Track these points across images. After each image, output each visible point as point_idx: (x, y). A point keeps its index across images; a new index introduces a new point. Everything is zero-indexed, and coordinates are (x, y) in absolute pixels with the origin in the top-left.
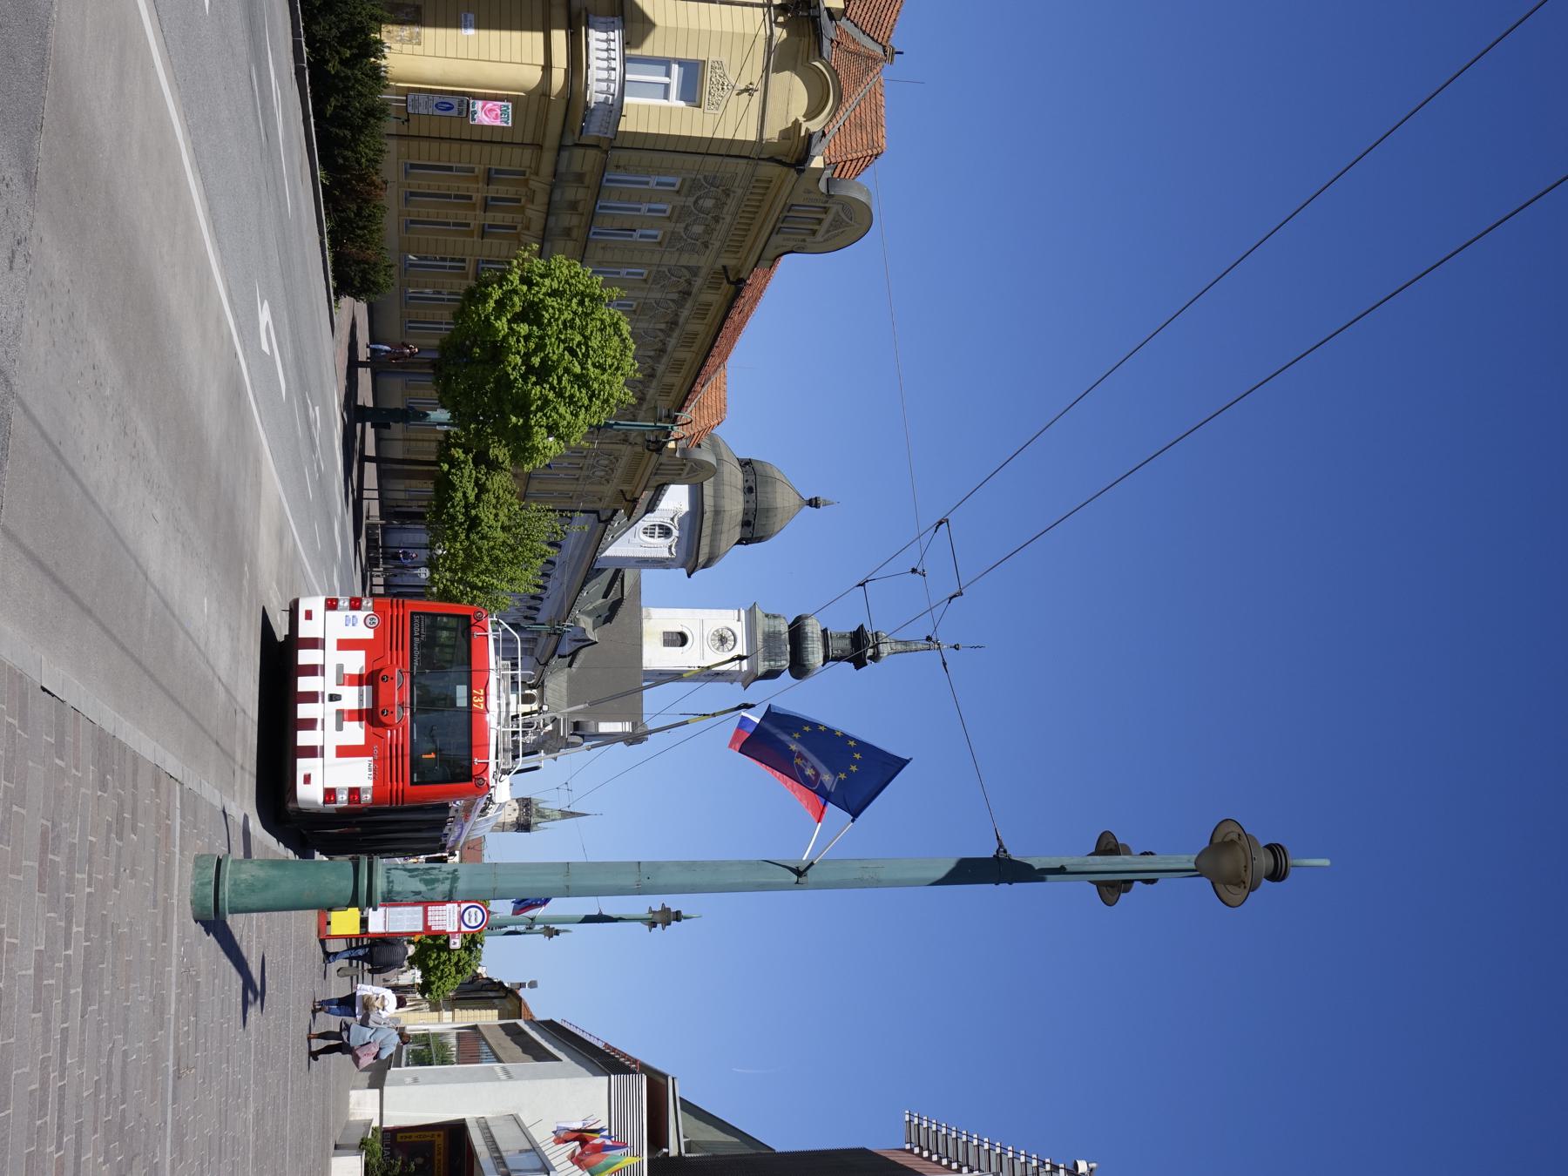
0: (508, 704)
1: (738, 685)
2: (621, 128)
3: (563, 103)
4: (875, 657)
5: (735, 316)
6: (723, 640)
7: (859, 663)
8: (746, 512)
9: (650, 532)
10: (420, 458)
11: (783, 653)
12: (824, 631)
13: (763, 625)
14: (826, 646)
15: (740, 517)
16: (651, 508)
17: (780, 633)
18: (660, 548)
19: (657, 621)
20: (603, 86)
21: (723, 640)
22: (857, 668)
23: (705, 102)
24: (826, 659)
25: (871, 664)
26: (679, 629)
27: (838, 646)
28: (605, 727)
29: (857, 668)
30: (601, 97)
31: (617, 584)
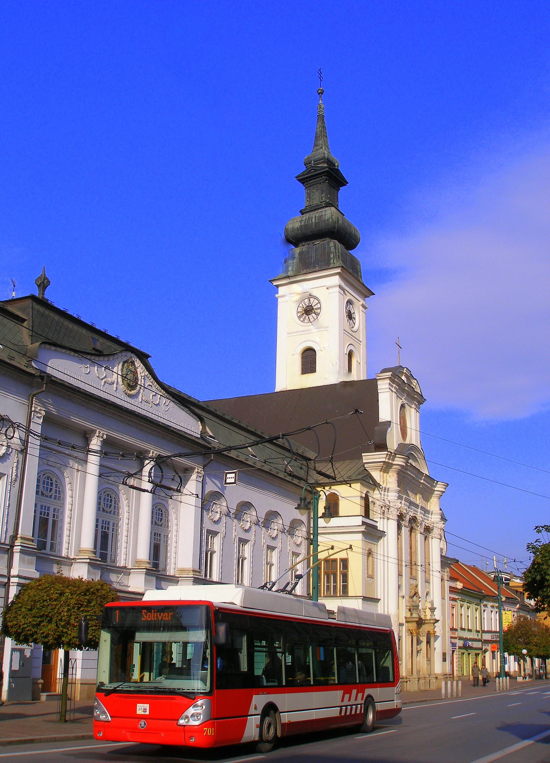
6: (308, 311)
12: (302, 212)
21: (308, 311)
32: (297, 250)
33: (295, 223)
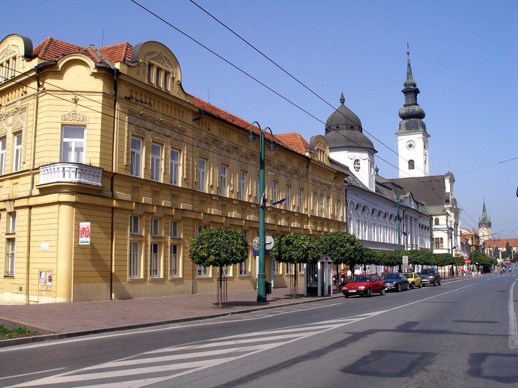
0: (129, 58)
1: (429, 139)
2: (98, 165)
3: (82, 196)
4: (415, 85)
5: (224, 117)
6: (410, 146)
7: (416, 92)
8: (347, 129)
9: (358, 169)
10: (279, 308)
11: (415, 121)
13: (403, 129)
14: (410, 105)
15: (350, 131)
16: (347, 169)
17: (406, 123)
18: (365, 165)
19: (404, 173)
20: (67, 174)
21: (410, 146)
22: (419, 92)
23: (83, 123)
24: (416, 104)
25: (418, 87)
26: (408, 163)
27: (411, 101)
28: (113, 295)
29: (419, 92)
30: (73, 174)
31: (386, 185)
32: (405, 122)
33: (404, 111)
